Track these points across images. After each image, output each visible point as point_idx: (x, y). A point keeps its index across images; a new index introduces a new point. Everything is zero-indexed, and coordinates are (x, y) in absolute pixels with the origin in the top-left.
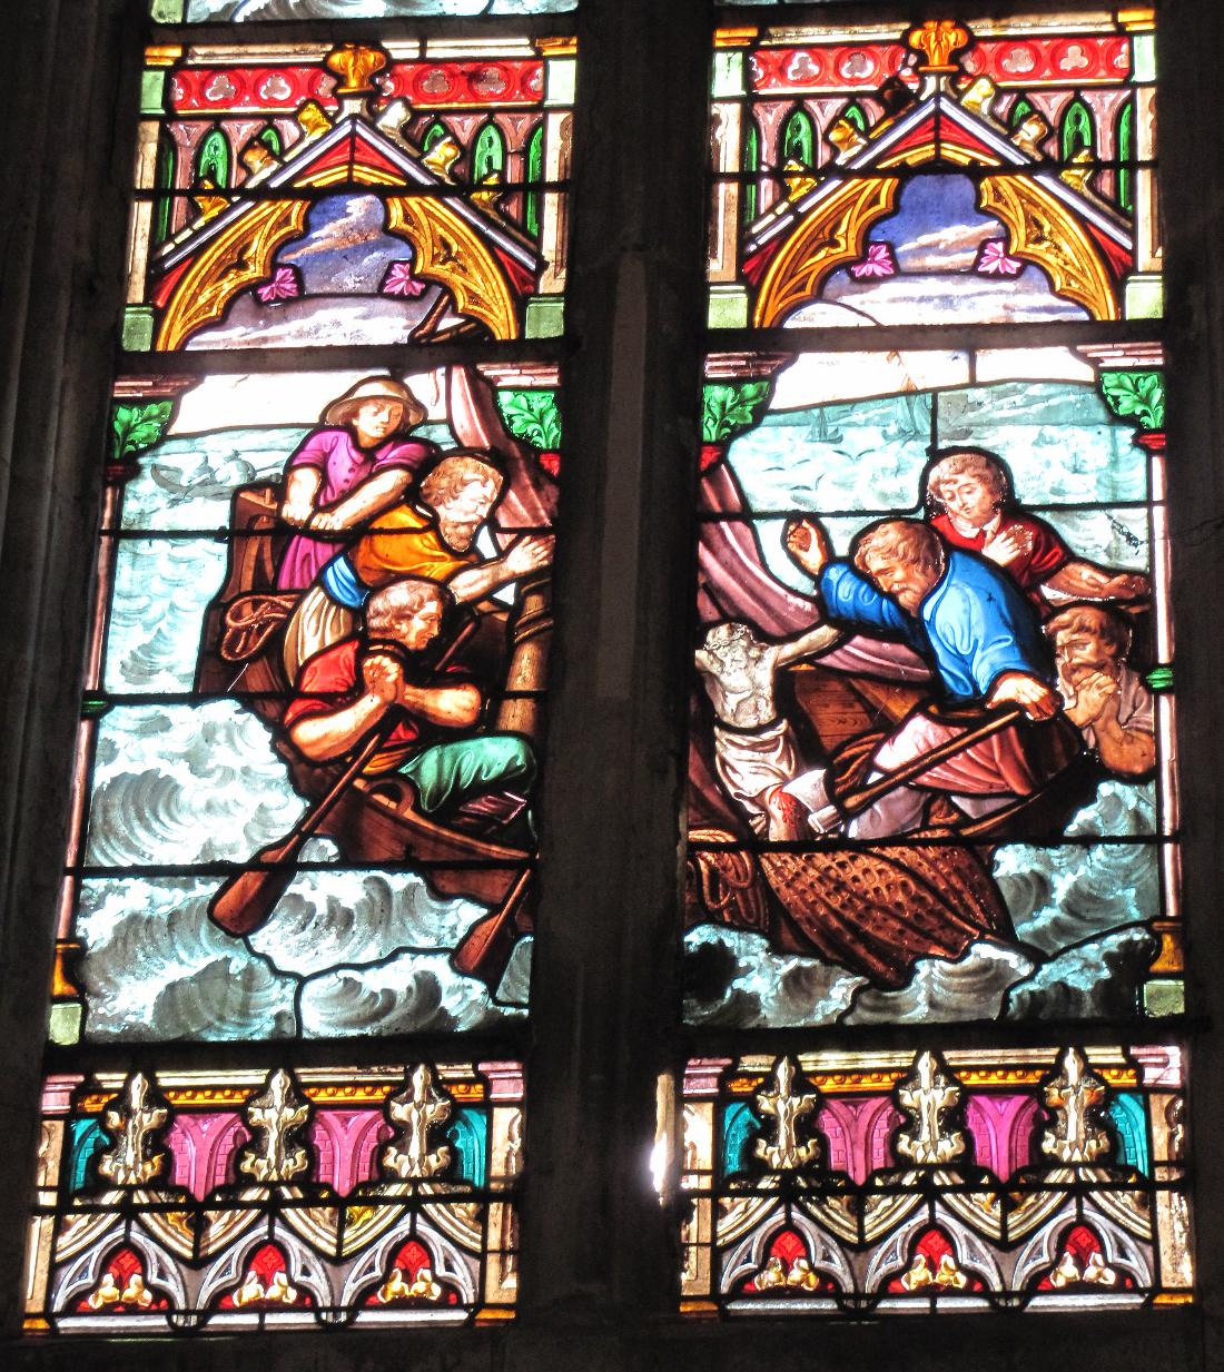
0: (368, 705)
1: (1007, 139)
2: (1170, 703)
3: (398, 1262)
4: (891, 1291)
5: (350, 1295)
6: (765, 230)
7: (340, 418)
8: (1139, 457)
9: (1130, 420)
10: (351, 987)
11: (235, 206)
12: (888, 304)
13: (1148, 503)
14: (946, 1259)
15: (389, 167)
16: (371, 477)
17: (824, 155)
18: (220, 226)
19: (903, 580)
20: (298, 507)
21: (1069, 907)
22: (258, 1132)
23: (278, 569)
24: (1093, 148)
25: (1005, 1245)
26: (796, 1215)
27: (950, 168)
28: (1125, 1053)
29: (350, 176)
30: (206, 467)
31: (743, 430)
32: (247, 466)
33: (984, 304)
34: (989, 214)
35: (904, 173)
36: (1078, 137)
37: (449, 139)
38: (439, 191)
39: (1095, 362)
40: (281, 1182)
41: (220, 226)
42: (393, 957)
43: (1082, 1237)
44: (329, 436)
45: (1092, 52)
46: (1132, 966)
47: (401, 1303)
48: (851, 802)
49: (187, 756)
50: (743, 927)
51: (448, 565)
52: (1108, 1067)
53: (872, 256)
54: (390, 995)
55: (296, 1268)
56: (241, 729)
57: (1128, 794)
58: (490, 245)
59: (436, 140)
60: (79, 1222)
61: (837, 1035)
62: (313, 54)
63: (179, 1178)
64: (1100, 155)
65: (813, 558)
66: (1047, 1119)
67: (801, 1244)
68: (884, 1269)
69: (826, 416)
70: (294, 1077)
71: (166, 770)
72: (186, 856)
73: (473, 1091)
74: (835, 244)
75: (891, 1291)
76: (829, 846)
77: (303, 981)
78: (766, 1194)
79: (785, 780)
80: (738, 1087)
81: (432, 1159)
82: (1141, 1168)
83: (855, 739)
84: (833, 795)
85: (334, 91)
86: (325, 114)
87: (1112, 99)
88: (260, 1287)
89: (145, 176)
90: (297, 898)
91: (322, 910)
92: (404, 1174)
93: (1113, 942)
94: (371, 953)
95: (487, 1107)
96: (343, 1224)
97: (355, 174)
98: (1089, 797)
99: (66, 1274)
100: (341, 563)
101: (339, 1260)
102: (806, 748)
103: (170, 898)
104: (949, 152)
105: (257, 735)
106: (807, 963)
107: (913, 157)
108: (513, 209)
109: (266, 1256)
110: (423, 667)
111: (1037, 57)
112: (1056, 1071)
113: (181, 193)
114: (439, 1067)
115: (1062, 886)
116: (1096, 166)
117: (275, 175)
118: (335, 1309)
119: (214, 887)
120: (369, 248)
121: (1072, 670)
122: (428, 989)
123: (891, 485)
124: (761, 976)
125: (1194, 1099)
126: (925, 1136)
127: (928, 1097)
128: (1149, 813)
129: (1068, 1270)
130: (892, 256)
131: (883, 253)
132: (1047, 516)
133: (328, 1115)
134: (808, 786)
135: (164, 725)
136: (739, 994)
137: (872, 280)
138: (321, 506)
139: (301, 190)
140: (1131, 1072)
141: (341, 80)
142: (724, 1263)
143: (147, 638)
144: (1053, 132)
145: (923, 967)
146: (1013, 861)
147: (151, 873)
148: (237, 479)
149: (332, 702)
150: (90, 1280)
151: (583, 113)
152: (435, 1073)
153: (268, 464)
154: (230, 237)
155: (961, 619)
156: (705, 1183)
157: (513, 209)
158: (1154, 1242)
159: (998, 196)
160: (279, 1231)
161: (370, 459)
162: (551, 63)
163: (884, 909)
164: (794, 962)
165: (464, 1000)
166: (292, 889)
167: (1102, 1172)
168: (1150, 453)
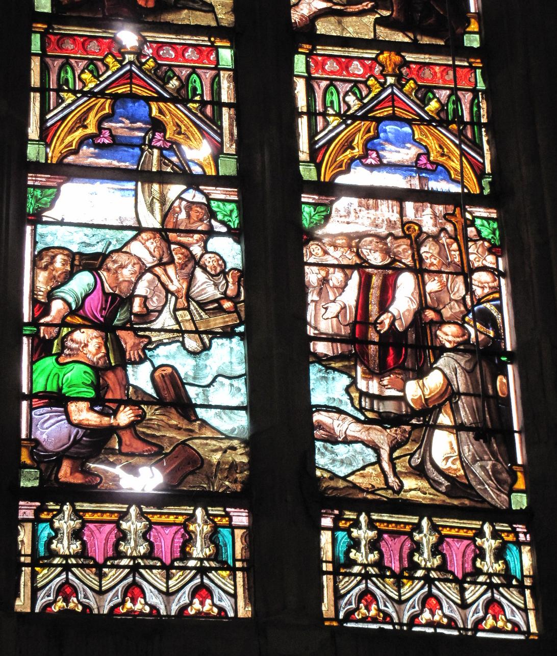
2: (28, 341)
3: (129, 595)
4: (416, 623)
5: (39, 607)
6: (322, 138)
11: (78, 99)
15: (411, 111)
18: (73, 108)
24: (202, 95)
26: (71, 576)
28: (225, 511)
29: (131, 90)
35: (115, 97)
36: (195, 89)
37: (176, 78)
38: (174, 100)
39: (207, 196)
40: (368, 565)
41: (73, 108)
43: (68, 590)
52: (503, 531)
55: (81, 596)
60: (178, 574)
62: (371, 54)
63: (157, 552)
64: (205, 98)
66: (189, 540)
67: (74, 591)
68: (111, 604)
70: (207, 511)
73: (113, 516)
74: (353, 148)
75: (416, 623)
80: (44, 516)
82: (518, 576)
85: (382, 72)
86: (379, 82)
88: (64, 604)
89: (35, 79)
92: (359, 561)
96: (168, 577)
97: (134, 89)
99: (41, 594)
101: (400, 602)
104: (398, 112)
107: (121, 90)
109: (134, 591)
112: (191, 518)
113: (53, 90)
114: (209, 508)
116: (203, 103)
117: (97, 86)
118: (401, 624)
125: (252, 532)
131: (374, 155)
133: (91, 526)
139: (110, 94)
140: (227, 519)
142: (38, 595)
144: (184, 85)
150: (481, 614)
151: (239, 74)
152: (207, 511)
156: (28, 560)
160: (138, 579)
162: (220, 50)
167: (375, 569)
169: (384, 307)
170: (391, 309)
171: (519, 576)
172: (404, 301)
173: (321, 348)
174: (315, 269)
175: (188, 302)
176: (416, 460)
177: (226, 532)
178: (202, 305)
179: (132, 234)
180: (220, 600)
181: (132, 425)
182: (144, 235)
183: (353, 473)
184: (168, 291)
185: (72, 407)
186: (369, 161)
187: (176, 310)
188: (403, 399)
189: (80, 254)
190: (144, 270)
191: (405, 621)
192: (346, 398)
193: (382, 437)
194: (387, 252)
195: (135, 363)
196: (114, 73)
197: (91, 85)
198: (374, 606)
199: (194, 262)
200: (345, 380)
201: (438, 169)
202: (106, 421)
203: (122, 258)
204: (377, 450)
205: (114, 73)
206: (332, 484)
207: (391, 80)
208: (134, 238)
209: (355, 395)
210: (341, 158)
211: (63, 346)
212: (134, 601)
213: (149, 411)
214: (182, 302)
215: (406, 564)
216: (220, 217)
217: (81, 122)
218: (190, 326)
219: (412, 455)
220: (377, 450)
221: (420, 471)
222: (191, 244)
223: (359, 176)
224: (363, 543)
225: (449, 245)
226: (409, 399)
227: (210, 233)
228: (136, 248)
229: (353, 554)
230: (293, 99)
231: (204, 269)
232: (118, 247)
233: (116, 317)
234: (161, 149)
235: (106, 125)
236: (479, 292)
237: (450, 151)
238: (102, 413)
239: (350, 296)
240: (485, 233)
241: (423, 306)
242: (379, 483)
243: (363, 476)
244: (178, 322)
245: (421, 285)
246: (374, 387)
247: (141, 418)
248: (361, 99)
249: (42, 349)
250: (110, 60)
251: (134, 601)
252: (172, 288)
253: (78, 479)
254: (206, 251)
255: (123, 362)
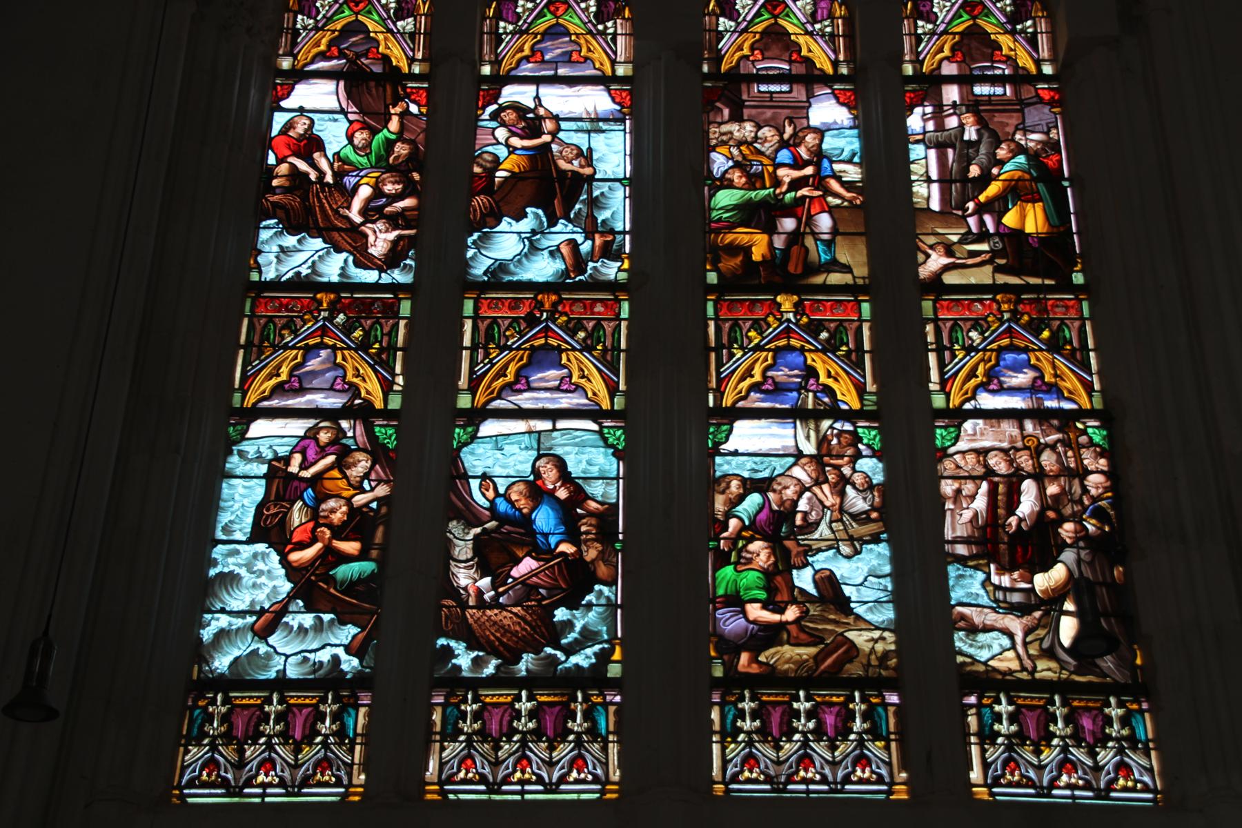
0: (319, 546)
1: (572, 337)
7: (311, 434)
8: (614, 460)
9: (612, 446)
10: (306, 659)
12: (525, 400)
13: (617, 478)
14: (528, 770)
16: (323, 457)
17: (503, 342)
19: (524, 505)
20: (294, 468)
21: (580, 633)
22: (268, 715)
23: (285, 491)
25: (834, 764)
27: (793, 349)
30: (258, 451)
31: (466, 444)
32: (275, 452)
33: (566, 401)
34: (565, 367)
42: (323, 647)
44: (307, 441)
45: (606, 306)
46: (604, 658)
47: (749, 781)
48: (501, 590)
49: (245, 565)
50: (457, 639)
51: (352, 492)
53: (522, 382)
54: (321, 663)
56: (268, 555)
57: (605, 590)
58: (376, 371)
59: (356, 329)
61: (491, 682)
65: (491, 494)
69: (498, 441)
71: (237, 570)
72: (243, 606)
74: (752, 376)
76: (491, 607)
77: (287, 657)
78: (462, 742)
79: (476, 581)
81: (475, 726)
83: (503, 566)
84: (494, 586)
87: (1077, 324)
90: (287, 623)
91: (295, 628)
93: (597, 648)
94: (315, 646)
95: (357, 707)
98: (591, 590)
100: (310, 490)
102: (483, 571)
103: (238, 622)
105: (275, 557)
106: (481, 654)
108: (384, 356)
110: (340, 532)
111: (585, 307)
115: (578, 626)
119: (254, 618)
120: (328, 370)
121: (586, 541)
122: (336, 660)
123: (520, 467)
124: (464, 659)
126: (523, 720)
127: (525, 706)
128: (613, 597)
129: (574, 774)
130: (528, 383)
131: (996, 381)
132: (580, 481)
134: (485, 582)
135: (237, 552)
136: (454, 665)
137: (520, 391)
138: (303, 466)
141: (320, 303)
143: (232, 518)
145: (525, 656)
146: (561, 614)
147: (230, 613)
148: (270, 456)
149: (301, 546)
153: (283, 451)
154: (274, 364)
155: (544, 519)
157: (384, 356)
158: (607, 764)
159: (569, 360)
161: (323, 452)
163: (511, 632)
164: (476, 653)
165: (350, 664)
166: (285, 619)
168: (619, 459)
169: (1011, 512)
170: (1018, 512)
171: (1143, 738)
172: (1028, 504)
173: (961, 550)
174: (949, 481)
175: (841, 514)
176: (1046, 645)
177: (880, 710)
178: (854, 517)
179: (791, 460)
180: (878, 768)
181: (797, 621)
182: (803, 461)
183: (992, 658)
184: (824, 506)
185: (749, 607)
186: (992, 387)
187: (831, 522)
188: (1033, 590)
189: (751, 479)
190: (803, 489)
191: (1045, 783)
192: (982, 592)
193: (1016, 625)
194: (1011, 462)
195: (799, 568)
196: (775, 329)
197: (756, 341)
198: (1017, 773)
199: (844, 481)
200: (980, 576)
201: (1054, 390)
202: (776, 617)
203: (785, 481)
204: (1011, 636)
205: (775, 329)
206: (974, 668)
207: (1006, 316)
208: (795, 464)
209: (990, 588)
210: (966, 387)
211: (739, 557)
212: (806, 771)
213: (814, 610)
214: (836, 514)
215: (1042, 734)
216: (865, 441)
217: (748, 373)
218: (842, 535)
219: (1042, 640)
220: (1011, 636)
221: (1049, 654)
222: (842, 466)
223: (987, 401)
224: (1004, 716)
225: (1065, 453)
226: (1037, 589)
227: (858, 455)
228: (798, 472)
229: (996, 727)
230: (1098, 358)
231: (854, 485)
232: (782, 471)
233: (780, 527)
234: (815, 392)
235: (770, 374)
236: (1093, 492)
237: (1063, 373)
238: (774, 611)
239: (980, 503)
240: (1097, 439)
241: (1044, 507)
242: (1015, 665)
243: (1000, 660)
244: (833, 532)
245: (1042, 490)
246: (1006, 581)
247: (804, 614)
248: (982, 333)
249: (722, 559)
250: (771, 319)
251: (806, 771)
252: (827, 503)
253: (755, 669)
254: (854, 471)
255: (789, 568)
